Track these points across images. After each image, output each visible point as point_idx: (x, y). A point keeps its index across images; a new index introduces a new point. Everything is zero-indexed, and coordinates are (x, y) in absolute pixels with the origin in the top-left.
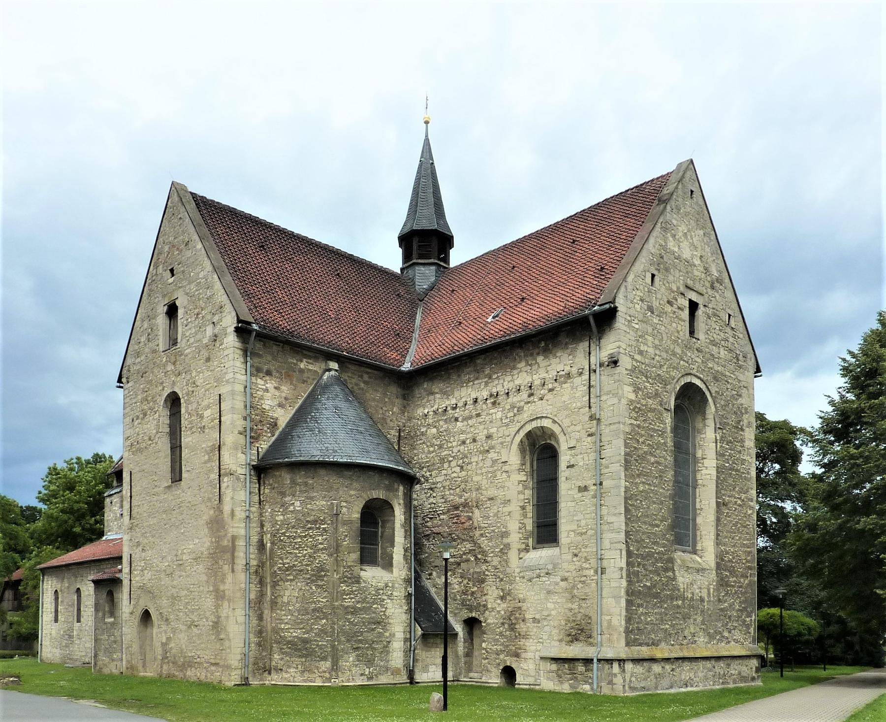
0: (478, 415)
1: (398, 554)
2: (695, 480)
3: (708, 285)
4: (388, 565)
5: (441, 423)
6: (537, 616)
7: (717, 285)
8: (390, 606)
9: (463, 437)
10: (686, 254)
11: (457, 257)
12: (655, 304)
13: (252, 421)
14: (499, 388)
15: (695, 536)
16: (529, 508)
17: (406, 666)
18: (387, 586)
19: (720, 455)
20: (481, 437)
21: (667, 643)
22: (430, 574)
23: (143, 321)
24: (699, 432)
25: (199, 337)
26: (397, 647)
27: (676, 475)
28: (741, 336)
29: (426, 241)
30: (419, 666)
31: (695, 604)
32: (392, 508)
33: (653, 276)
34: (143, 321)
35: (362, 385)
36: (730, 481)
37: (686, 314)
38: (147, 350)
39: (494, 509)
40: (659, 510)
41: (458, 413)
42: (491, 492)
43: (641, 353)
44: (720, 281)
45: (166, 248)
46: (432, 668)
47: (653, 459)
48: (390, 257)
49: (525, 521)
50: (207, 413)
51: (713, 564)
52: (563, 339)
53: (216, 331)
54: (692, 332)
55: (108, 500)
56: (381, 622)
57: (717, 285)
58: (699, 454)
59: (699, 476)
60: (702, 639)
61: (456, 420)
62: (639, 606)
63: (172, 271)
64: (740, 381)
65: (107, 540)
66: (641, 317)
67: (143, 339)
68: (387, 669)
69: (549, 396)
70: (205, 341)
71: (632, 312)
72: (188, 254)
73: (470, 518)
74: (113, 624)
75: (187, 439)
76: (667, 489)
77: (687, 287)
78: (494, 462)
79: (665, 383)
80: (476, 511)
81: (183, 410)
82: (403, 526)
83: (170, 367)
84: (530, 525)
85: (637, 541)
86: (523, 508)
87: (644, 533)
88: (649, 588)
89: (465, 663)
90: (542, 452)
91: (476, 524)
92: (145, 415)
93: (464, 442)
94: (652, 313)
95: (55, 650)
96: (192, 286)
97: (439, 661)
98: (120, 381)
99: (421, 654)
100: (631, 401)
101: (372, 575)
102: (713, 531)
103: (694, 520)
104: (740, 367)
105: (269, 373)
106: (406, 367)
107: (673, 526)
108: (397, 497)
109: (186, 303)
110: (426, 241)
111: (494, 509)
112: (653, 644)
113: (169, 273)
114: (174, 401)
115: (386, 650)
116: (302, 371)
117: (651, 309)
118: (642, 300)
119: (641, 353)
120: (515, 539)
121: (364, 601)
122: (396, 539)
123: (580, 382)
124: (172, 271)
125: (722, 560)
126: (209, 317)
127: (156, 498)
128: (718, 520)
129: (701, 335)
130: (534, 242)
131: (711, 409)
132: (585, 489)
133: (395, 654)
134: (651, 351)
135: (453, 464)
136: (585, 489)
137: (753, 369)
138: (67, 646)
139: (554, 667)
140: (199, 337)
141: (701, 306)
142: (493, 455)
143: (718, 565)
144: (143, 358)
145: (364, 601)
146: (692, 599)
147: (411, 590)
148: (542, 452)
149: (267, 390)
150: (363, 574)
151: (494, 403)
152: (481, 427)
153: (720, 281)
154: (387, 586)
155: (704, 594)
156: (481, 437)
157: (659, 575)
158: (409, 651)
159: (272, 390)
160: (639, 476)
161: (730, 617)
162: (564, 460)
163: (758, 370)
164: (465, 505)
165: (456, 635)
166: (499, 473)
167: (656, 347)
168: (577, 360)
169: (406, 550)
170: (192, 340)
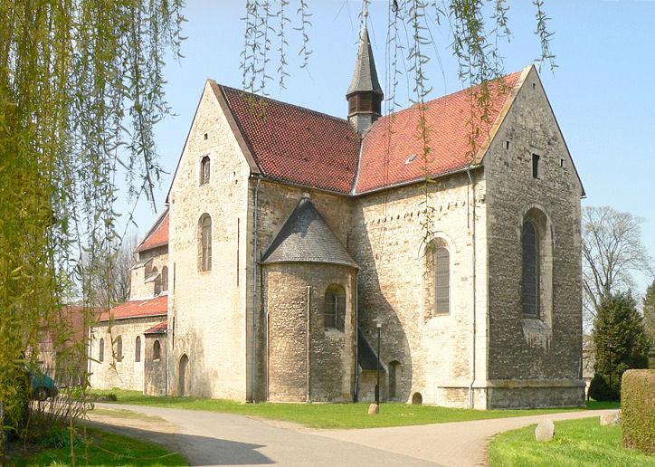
0: (400, 227)
1: (348, 320)
2: (539, 270)
3: (546, 143)
4: (341, 327)
5: (376, 231)
6: (436, 360)
7: (552, 141)
8: (342, 353)
9: (389, 241)
10: (531, 125)
11: (385, 107)
12: (510, 160)
13: (258, 234)
14: (413, 210)
15: (539, 308)
16: (432, 289)
17: (353, 392)
18: (341, 340)
19: (554, 254)
20: (401, 242)
21: (518, 378)
22: (368, 332)
23: (185, 164)
24: (542, 238)
25: (225, 180)
26: (347, 379)
27: (524, 270)
28: (571, 173)
29: (368, 100)
30: (361, 392)
31: (537, 352)
32: (344, 289)
33: (508, 143)
34: (185, 164)
35: (324, 206)
36: (563, 269)
37: (530, 165)
38: (187, 184)
39: (410, 290)
40: (513, 294)
41: (387, 225)
42: (408, 279)
43: (500, 192)
44: (555, 139)
45: (203, 120)
46: (369, 394)
47: (508, 260)
48: (339, 109)
49: (430, 298)
50: (230, 229)
51: (551, 326)
52: (452, 181)
53: (236, 178)
54: (535, 175)
55: (134, 272)
56: (338, 363)
57: (552, 141)
58: (542, 253)
59: (541, 268)
60: (541, 378)
61: (385, 229)
62: (498, 354)
63: (206, 135)
64: (570, 203)
65: (134, 302)
66: (499, 170)
67: (185, 176)
68: (341, 394)
69: (444, 218)
70: (229, 183)
71: (494, 168)
72: (218, 126)
73: (394, 295)
74: (159, 363)
75: (216, 246)
76: (517, 278)
77: (531, 146)
78: (409, 258)
79: (516, 210)
80: (398, 291)
81: (213, 226)
82: (351, 301)
83: (203, 197)
84: (432, 300)
85: (497, 312)
86: (428, 289)
87: (501, 307)
88: (506, 342)
89: (390, 391)
90: (436, 250)
91: (398, 300)
92: (186, 226)
93: (390, 245)
94: (508, 166)
95: (100, 382)
96: (221, 146)
97: (373, 389)
98: (167, 201)
99: (363, 385)
100: (493, 224)
101: (332, 334)
102: (551, 303)
103: (539, 297)
104: (571, 193)
105: (268, 203)
106: (354, 193)
107: (523, 300)
108: (347, 282)
109: (216, 158)
110: (368, 100)
111: (410, 290)
112: (507, 378)
113: (203, 137)
114: (205, 220)
115: (340, 382)
116: (287, 200)
117: (507, 164)
118: (500, 159)
119: (500, 192)
120: (421, 310)
121: (326, 350)
122: (347, 310)
123: (462, 211)
124: (206, 135)
125: (557, 323)
126: (231, 168)
127: (193, 281)
128: (554, 296)
129: (541, 176)
130: (437, 106)
131: (549, 222)
132: (466, 279)
133: (591, 364)
134: (507, 191)
135: (383, 258)
136: (466, 279)
137: (579, 194)
138: (111, 379)
139: (446, 392)
140: (225, 180)
141: (542, 158)
142: (408, 254)
143: (554, 326)
144: (184, 189)
145: (326, 350)
146: (535, 349)
147: (356, 343)
148: (436, 250)
149: (266, 214)
150: (326, 333)
151: (410, 220)
152: (401, 235)
153: (555, 139)
154: (341, 340)
155: (544, 345)
156: (401, 242)
157: (512, 334)
158: (355, 383)
159: (269, 214)
160: (499, 271)
161: (563, 360)
162: (452, 260)
163: (583, 194)
164: (391, 286)
165: (385, 372)
166: (412, 266)
167: (510, 188)
168: (460, 196)
169: (352, 317)
170: (219, 182)
